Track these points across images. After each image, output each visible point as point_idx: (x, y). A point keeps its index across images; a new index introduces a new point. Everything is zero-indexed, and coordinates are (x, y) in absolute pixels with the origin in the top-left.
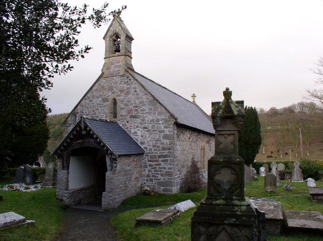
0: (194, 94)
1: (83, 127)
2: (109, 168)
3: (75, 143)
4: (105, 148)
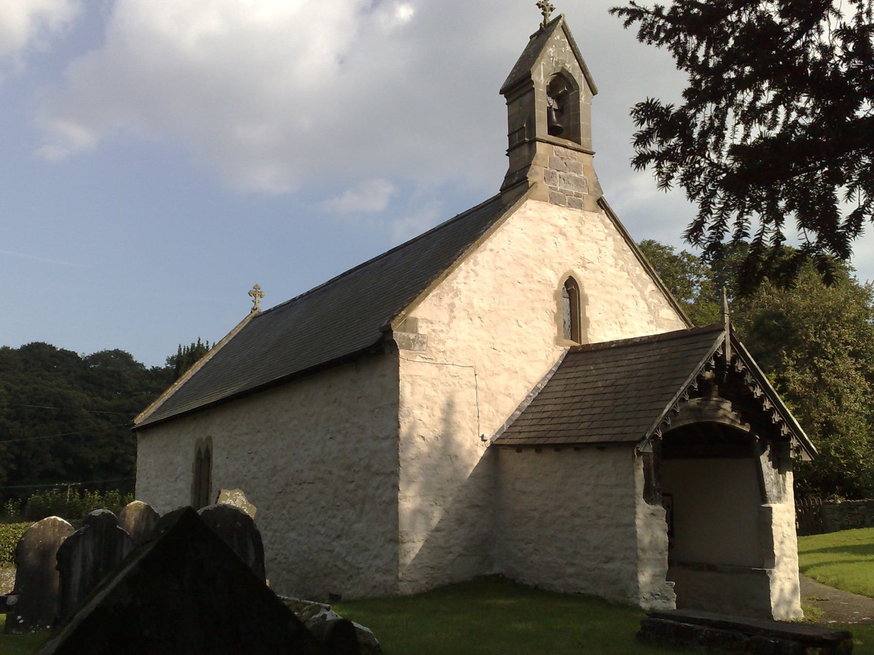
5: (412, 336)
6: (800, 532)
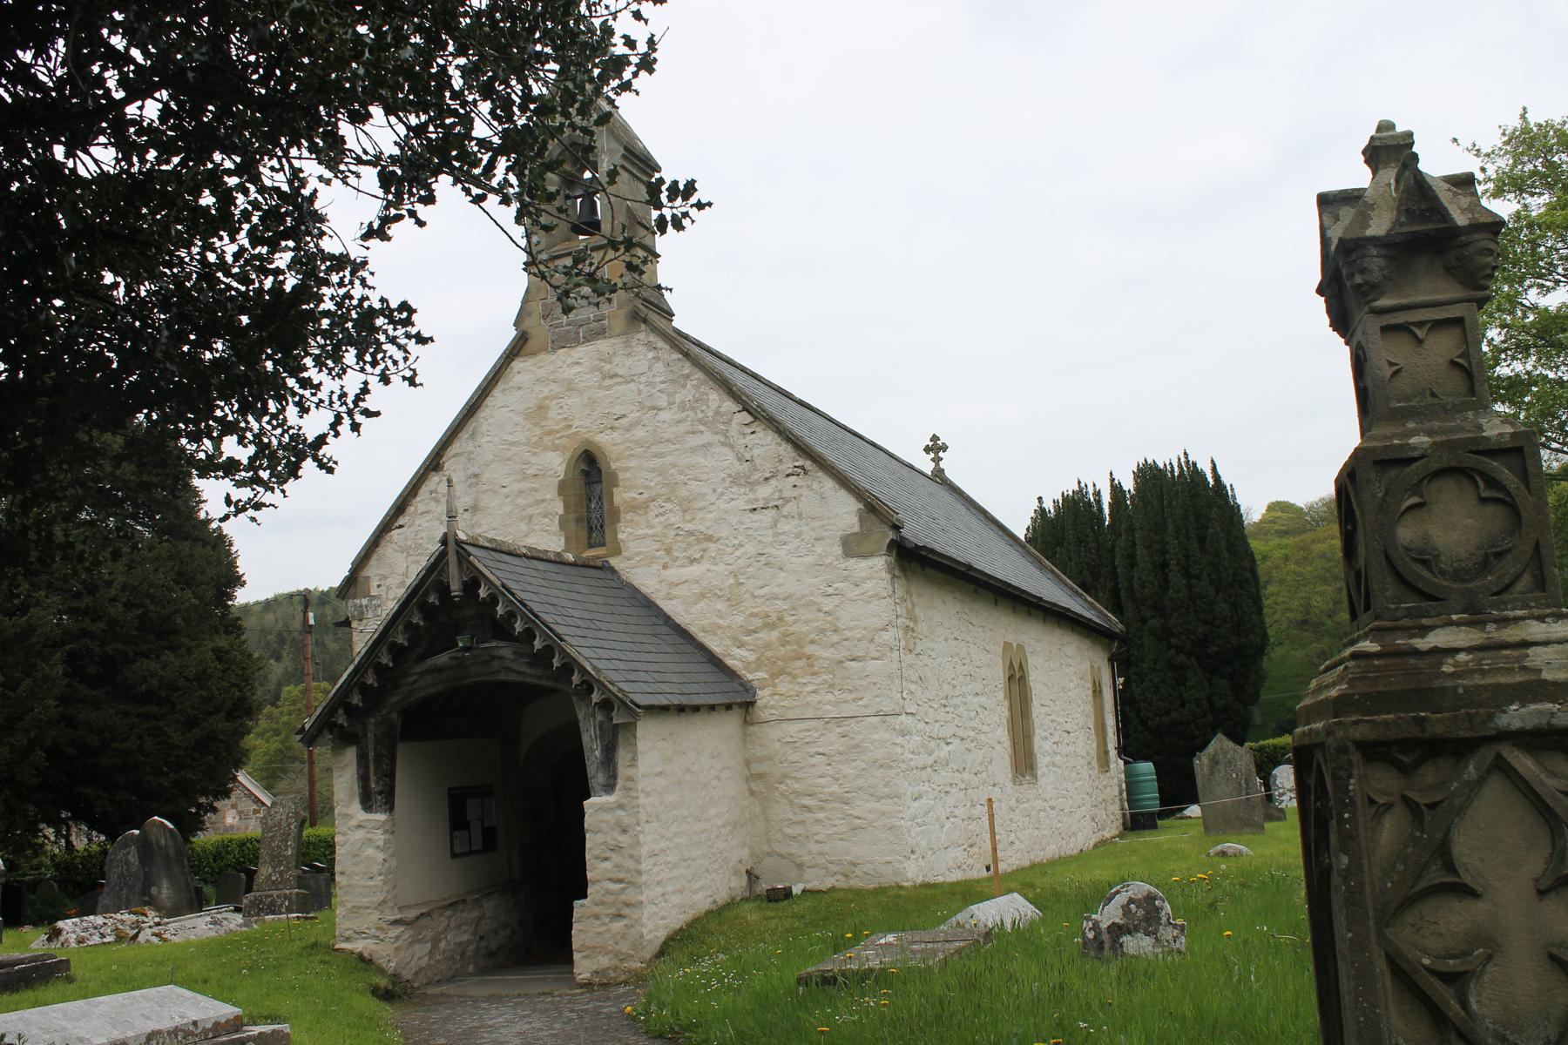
0: (935, 438)
1: (456, 588)
2: (596, 777)
3: (420, 668)
4: (576, 678)
5: (365, 601)
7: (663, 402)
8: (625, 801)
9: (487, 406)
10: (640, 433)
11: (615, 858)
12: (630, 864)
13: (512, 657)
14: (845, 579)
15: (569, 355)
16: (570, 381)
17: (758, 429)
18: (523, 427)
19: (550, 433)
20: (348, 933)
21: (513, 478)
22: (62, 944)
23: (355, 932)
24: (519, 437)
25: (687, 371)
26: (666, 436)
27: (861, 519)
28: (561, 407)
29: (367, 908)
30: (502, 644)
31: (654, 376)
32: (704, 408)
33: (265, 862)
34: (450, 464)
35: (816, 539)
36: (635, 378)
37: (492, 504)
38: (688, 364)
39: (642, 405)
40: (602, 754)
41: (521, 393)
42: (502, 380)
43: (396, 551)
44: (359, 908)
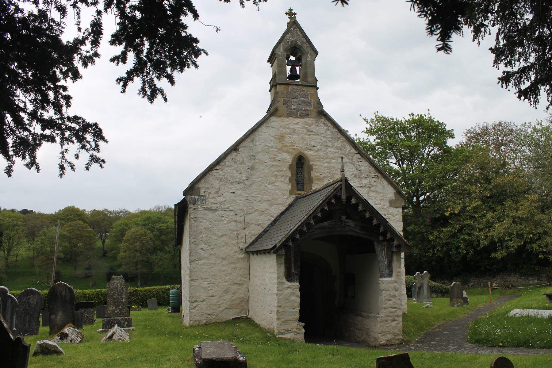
1: (344, 197)
5: (197, 197)
6: (406, 274)
7: (330, 144)
8: (397, 280)
9: (259, 131)
10: (322, 154)
11: (393, 300)
12: (399, 302)
13: (354, 226)
14: (390, 214)
15: (294, 120)
16: (294, 130)
17: (363, 161)
18: (274, 142)
19: (286, 146)
20: (282, 331)
21: (269, 160)
22: (71, 341)
23: (286, 330)
24: (272, 145)
25: (339, 136)
26: (331, 156)
27: (395, 196)
28: (290, 138)
29: (291, 320)
30: (350, 221)
31: (327, 135)
32: (345, 150)
33: (111, 304)
34: (241, 149)
35: (381, 200)
36: (320, 134)
37: (260, 168)
38: (339, 134)
39: (322, 144)
40: (387, 263)
41: (274, 129)
42: (266, 123)
43: (215, 179)
44: (287, 320)
